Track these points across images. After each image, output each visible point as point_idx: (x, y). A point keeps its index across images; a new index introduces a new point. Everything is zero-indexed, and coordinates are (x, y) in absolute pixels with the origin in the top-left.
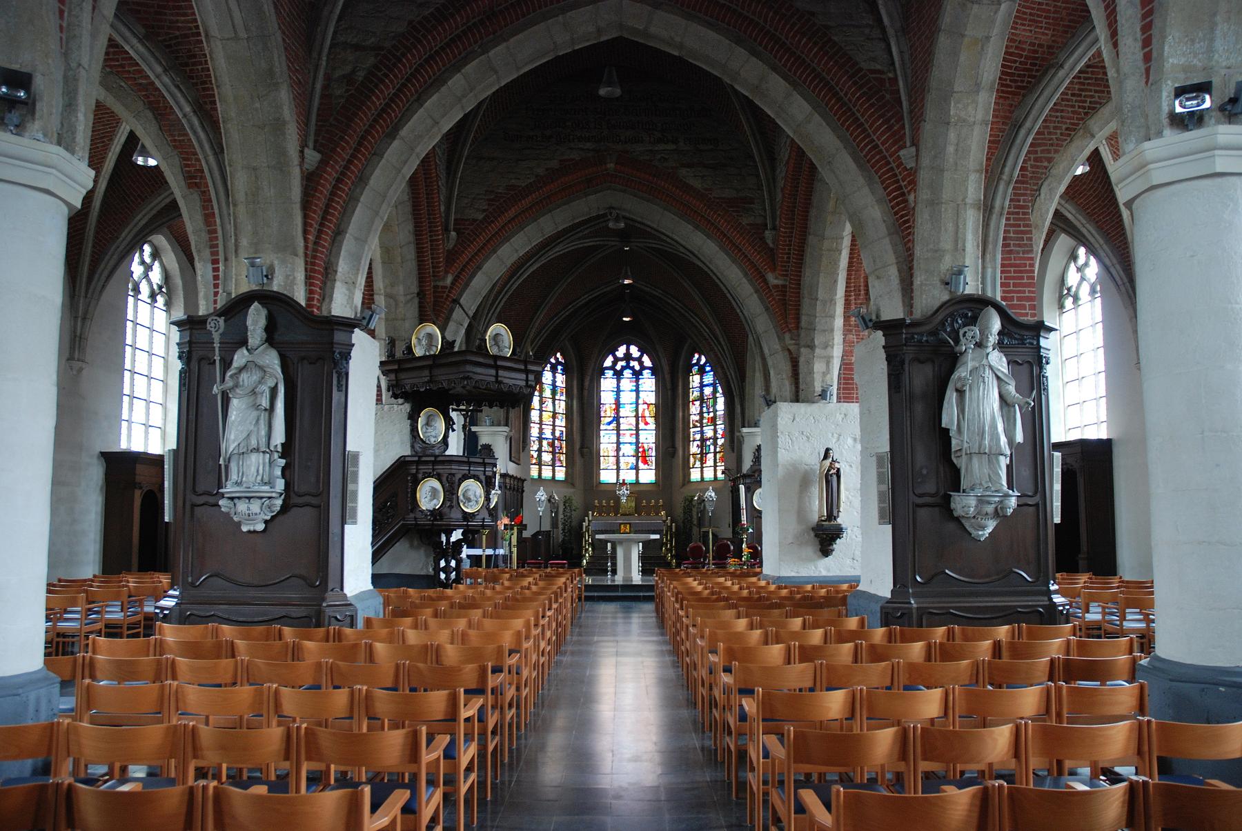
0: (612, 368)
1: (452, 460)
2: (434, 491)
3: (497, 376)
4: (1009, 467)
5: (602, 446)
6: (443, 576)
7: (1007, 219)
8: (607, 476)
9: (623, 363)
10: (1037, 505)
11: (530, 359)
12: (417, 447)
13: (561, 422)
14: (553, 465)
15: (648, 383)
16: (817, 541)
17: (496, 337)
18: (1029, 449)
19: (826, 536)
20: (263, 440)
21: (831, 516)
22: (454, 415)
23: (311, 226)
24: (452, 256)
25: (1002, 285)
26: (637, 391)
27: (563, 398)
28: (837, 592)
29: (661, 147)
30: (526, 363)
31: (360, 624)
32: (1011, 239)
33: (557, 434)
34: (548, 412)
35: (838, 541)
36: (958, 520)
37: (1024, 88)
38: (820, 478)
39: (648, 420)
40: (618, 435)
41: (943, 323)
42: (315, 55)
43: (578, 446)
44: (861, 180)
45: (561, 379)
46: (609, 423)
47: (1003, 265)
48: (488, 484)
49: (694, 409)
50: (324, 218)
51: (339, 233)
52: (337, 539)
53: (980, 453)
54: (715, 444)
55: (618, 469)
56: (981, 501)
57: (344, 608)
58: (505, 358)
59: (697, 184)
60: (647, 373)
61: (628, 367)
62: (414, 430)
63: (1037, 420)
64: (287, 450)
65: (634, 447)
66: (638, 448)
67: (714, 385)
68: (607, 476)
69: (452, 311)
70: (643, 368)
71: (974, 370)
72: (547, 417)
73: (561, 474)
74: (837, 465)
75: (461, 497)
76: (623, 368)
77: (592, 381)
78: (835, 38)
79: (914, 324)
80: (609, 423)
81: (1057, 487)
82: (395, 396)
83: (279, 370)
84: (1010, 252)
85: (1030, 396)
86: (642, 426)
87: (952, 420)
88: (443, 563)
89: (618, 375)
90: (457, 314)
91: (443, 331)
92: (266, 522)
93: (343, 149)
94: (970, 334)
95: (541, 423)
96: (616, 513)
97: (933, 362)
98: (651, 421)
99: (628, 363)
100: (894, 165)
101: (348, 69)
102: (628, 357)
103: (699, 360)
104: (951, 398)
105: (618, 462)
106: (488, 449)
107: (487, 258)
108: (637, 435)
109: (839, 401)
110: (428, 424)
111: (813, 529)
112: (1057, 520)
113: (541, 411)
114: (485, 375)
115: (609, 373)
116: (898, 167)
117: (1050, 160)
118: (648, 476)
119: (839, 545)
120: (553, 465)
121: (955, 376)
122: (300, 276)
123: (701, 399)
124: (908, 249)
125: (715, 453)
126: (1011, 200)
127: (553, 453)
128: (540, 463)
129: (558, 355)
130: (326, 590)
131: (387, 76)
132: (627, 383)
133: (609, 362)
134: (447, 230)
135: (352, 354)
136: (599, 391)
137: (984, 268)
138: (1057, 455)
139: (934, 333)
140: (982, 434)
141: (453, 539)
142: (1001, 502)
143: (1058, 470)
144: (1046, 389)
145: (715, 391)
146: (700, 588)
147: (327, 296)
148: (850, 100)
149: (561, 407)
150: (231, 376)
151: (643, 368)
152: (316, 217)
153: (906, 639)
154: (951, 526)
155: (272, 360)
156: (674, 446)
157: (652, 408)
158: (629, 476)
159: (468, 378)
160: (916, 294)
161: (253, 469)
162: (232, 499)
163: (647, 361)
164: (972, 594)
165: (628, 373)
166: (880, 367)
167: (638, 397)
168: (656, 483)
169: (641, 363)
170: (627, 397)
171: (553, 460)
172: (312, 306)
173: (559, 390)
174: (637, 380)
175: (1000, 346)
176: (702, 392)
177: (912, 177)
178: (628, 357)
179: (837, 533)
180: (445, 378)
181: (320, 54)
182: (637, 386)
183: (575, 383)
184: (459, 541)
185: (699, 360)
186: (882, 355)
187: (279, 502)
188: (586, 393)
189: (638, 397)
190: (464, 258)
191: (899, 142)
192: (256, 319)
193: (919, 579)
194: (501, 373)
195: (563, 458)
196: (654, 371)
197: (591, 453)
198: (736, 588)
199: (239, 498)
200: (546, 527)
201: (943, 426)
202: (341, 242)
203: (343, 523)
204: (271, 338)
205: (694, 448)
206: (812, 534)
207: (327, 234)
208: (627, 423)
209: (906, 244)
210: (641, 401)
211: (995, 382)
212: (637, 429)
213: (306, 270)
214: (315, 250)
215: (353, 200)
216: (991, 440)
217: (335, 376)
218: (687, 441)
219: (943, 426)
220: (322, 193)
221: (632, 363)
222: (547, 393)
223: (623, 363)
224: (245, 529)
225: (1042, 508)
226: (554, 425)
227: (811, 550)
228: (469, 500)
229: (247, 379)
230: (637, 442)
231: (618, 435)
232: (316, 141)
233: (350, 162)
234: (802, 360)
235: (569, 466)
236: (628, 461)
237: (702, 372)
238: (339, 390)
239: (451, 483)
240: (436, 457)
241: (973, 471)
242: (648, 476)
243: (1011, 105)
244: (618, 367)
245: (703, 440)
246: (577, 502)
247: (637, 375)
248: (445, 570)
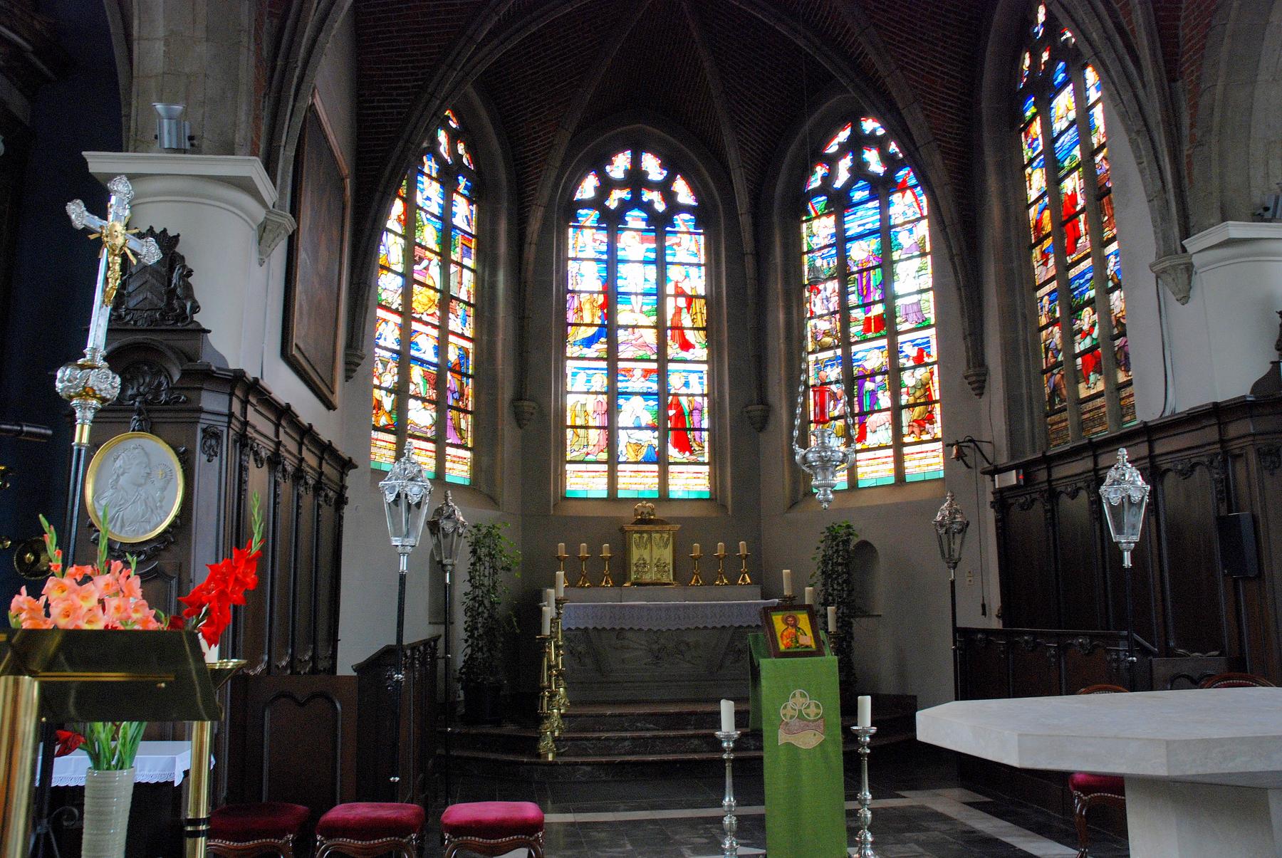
0: (598, 203)
5: (570, 400)
8: (583, 482)
9: (624, 194)
15: (688, 245)
26: (661, 263)
27: (470, 262)
33: (453, 356)
39: (691, 336)
40: (613, 373)
43: (506, 393)
45: (463, 211)
46: (589, 342)
49: (822, 301)
54: (896, 388)
55: (613, 462)
60: (683, 221)
61: (636, 202)
66: (663, 406)
68: (583, 482)
72: (423, 300)
73: (459, 470)
76: (625, 206)
77: (546, 227)
80: (589, 342)
86: (673, 350)
89: (612, 221)
96: (618, 583)
99: (636, 196)
102: (636, 179)
105: (612, 445)
108: (662, 374)
115: (589, 217)
118: (691, 481)
120: (439, 441)
123: (843, 273)
125: (896, 410)
127: (440, 405)
128: (400, 430)
132: (633, 244)
133: (588, 188)
136: (563, 260)
149: (464, 285)
151: (674, 206)
156: (763, 400)
157: (699, 305)
158: (638, 482)
165: (635, 219)
167: (662, 278)
168: (715, 499)
169: (669, 196)
171: (440, 424)
173: (459, 239)
174: (660, 237)
176: (843, 256)
178: (636, 179)
182: (661, 251)
183: (503, 227)
188: (531, 252)
189: (662, 278)
195: (466, 422)
196: (703, 217)
197: (543, 414)
200: (419, 629)
208: (637, 340)
210: (670, 289)
221: (647, 196)
223: (624, 194)
235: (483, 447)
242: (691, 481)
246: (510, 546)
247: (660, 224)
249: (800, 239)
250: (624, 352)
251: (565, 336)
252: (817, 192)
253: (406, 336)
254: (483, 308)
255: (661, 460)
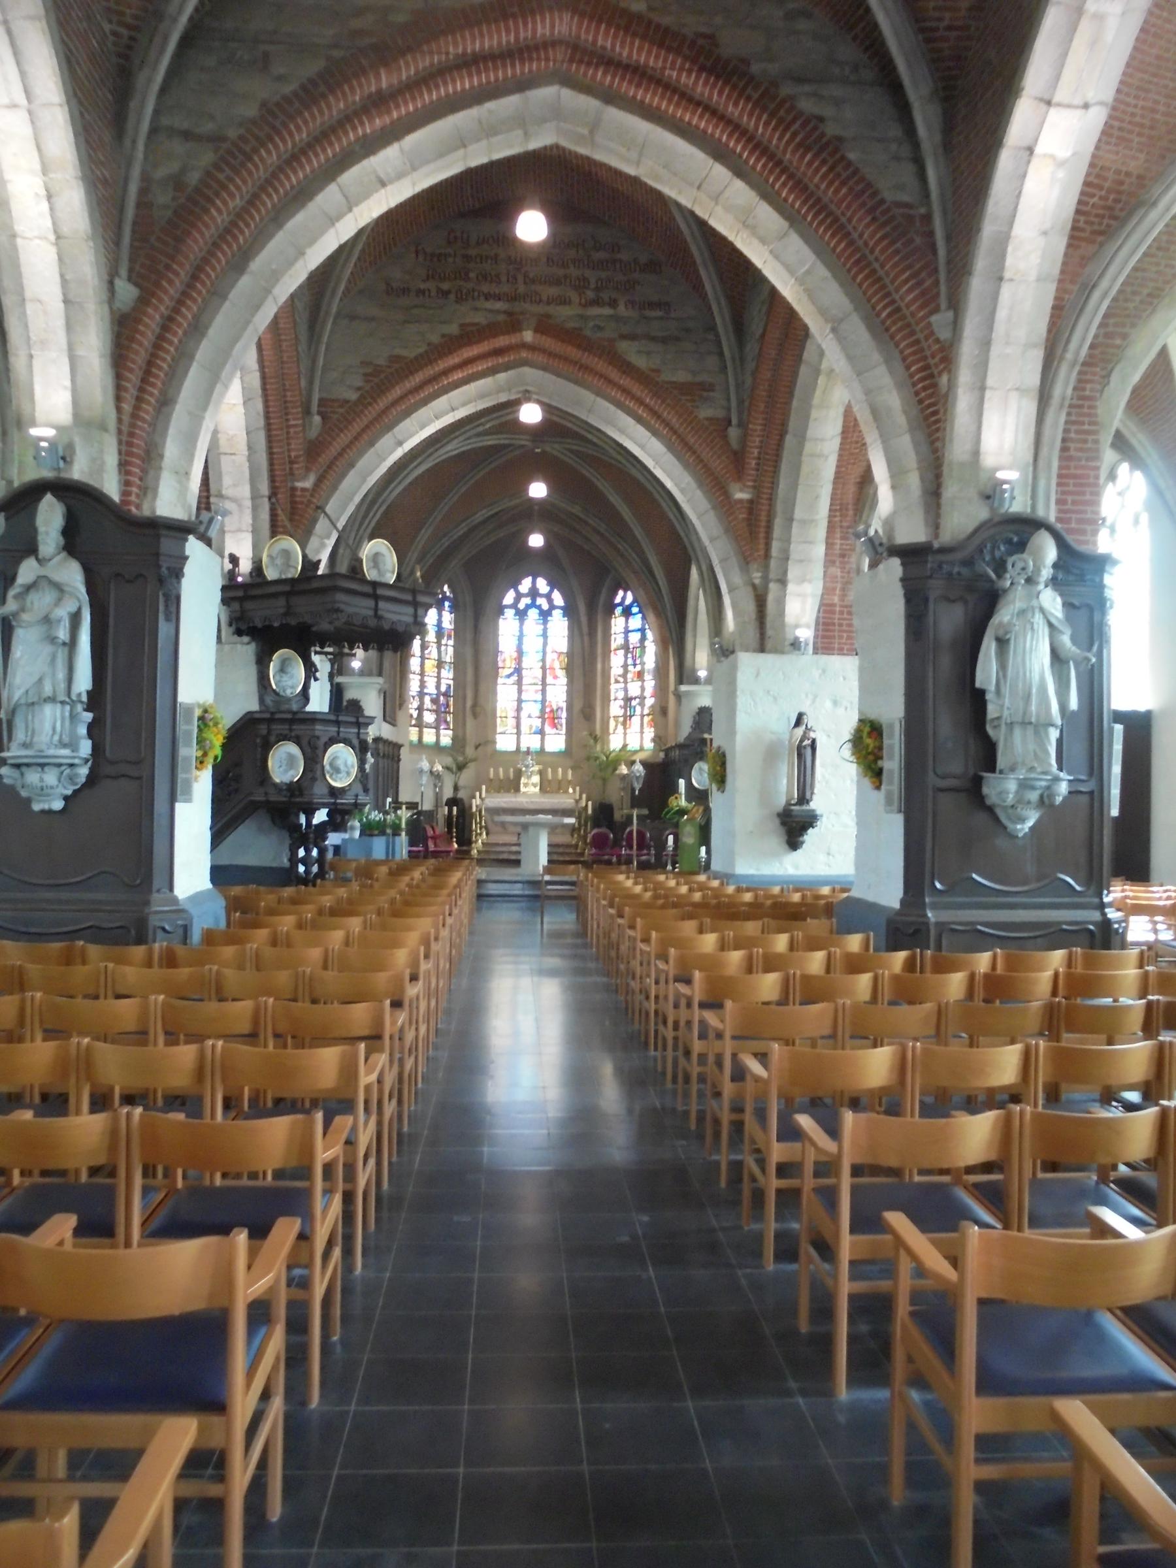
0: (514, 606)
1: (314, 718)
2: (291, 759)
3: (376, 609)
4: (1060, 742)
6: (301, 869)
7: (1069, 414)
8: (505, 743)
9: (528, 600)
10: (1091, 793)
11: (414, 593)
12: (269, 700)
13: (447, 675)
14: (437, 728)
15: (559, 625)
16: (781, 831)
17: (376, 558)
18: (1084, 718)
19: (795, 826)
20: (62, 686)
21: (803, 799)
22: (316, 659)
23: (126, 390)
24: (314, 450)
25: (1058, 502)
26: (545, 635)
27: (451, 642)
28: (818, 897)
29: (595, 311)
30: (414, 592)
31: (196, 936)
32: (1072, 440)
34: (430, 664)
35: (810, 831)
36: (990, 810)
37: (1101, 233)
38: (791, 749)
40: (520, 691)
41: (981, 551)
42: (127, 142)
44: (876, 357)
45: (448, 619)
46: (509, 676)
47: (1060, 476)
48: (362, 749)
49: (617, 661)
50: (143, 380)
51: (166, 402)
52: (165, 822)
53: (1025, 724)
54: (642, 704)
55: (518, 733)
56: (1024, 785)
57: (173, 916)
58: (386, 586)
59: (640, 362)
60: (557, 613)
61: (533, 605)
62: (263, 679)
63: (1094, 685)
64: (95, 700)
65: (539, 706)
67: (642, 630)
69: (314, 521)
70: (552, 607)
71: (1022, 613)
72: (430, 665)
73: (446, 739)
74: (812, 735)
75: (327, 767)
76: (528, 607)
78: (852, 156)
79: (943, 550)
80: (509, 676)
81: (1117, 769)
82: (239, 633)
83: (83, 590)
84: (1070, 458)
85: (1090, 649)
86: (549, 680)
87: (989, 677)
88: (301, 853)
89: (521, 614)
90: (322, 525)
91: (303, 548)
92: (66, 798)
93: (171, 282)
94: (1020, 565)
95: (422, 674)
97: (966, 602)
98: (562, 674)
99: (534, 600)
100: (920, 336)
101: (174, 167)
102: (534, 593)
103: (624, 598)
104: (988, 648)
105: (518, 726)
106: (355, 706)
107: (361, 453)
108: (544, 691)
109: (816, 652)
110: (282, 670)
111: (779, 815)
112: (1115, 812)
113: (423, 658)
114: (360, 608)
116: (927, 338)
117: (1125, 336)
118: (556, 742)
119: (810, 836)
121: (995, 620)
122: (111, 460)
123: (626, 647)
124: (935, 451)
125: (642, 716)
126: (1075, 389)
128: (420, 724)
129: (446, 588)
130: (150, 891)
131: (231, 180)
133: (509, 598)
134: (307, 412)
135: (186, 570)
137: (1035, 478)
138: (1119, 728)
139: (969, 563)
140: (1027, 698)
141: (315, 821)
142: (1048, 788)
143: (1118, 747)
144: (1108, 642)
145: (643, 638)
146: (638, 889)
147: (149, 489)
148: (866, 244)
149: (449, 655)
150: (16, 597)
151: (552, 607)
152: (133, 379)
153: (943, 967)
154: (981, 817)
155: (73, 575)
158: (531, 742)
159: (338, 610)
160: (945, 508)
161: (47, 727)
162: (18, 766)
163: (558, 599)
164: (1012, 906)
165: (533, 613)
166: (896, 607)
167: (545, 644)
170: (532, 644)
172: (128, 503)
174: (545, 622)
175: (1054, 582)
177: (946, 356)
178: (534, 593)
179: (810, 821)
180: (305, 609)
181: (134, 142)
182: (545, 630)
184: (323, 823)
185: (624, 598)
186: (898, 592)
187: (84, 771)
189: (545, 644)
190: (333, 450)
191: (930, 301)
192: (50, 517)
193: (938, 885)
194: (381, 604)
195: (449, 718)
196: (568, 611)
198: (684, 889)
199: (28, 765)
201: (978, 685)
202: (168, 417)
203: (173, 800)
204: (72, 542)
205: (616, 709)
206: (777, 821)
207: (149, 403)
208: (532, 673)
209: (932, 443)
210: (549, 649)
211: (1047, 630)
212: (544, 683)
213: (120, 453)
214: (132, 425)
215: (185, 357)
216: (1039, 705)
217: (161, 599)
218: (606, 699)
219: (978, 685)
220: (141, 344)
222: (431, 637)
224: (36, 807)
225: (1097, 798)
226: (439, 677)
227: (776, 840)
228: (337, 770)
229: (41, 601)
230: (544, 701)
231: (520, 691)
232: (131, 270)
233: (180, 302)
234: (771, 598)
236: (531, 721)
237: (627, 613)
238: (168, 619)
239: (314, 748)
240: (295, 713)
241: (1014, 747)
243: (1083, 258)
244: (521, 606)
245: (628, 700)
247: (545, 615)
248: (305, 861)
249: (495, 726)
250: (525, 681)
251: (497, 673)
252: (619, 605)
253: (422, 684)
254: (458, 665)
255: (541, 732)
